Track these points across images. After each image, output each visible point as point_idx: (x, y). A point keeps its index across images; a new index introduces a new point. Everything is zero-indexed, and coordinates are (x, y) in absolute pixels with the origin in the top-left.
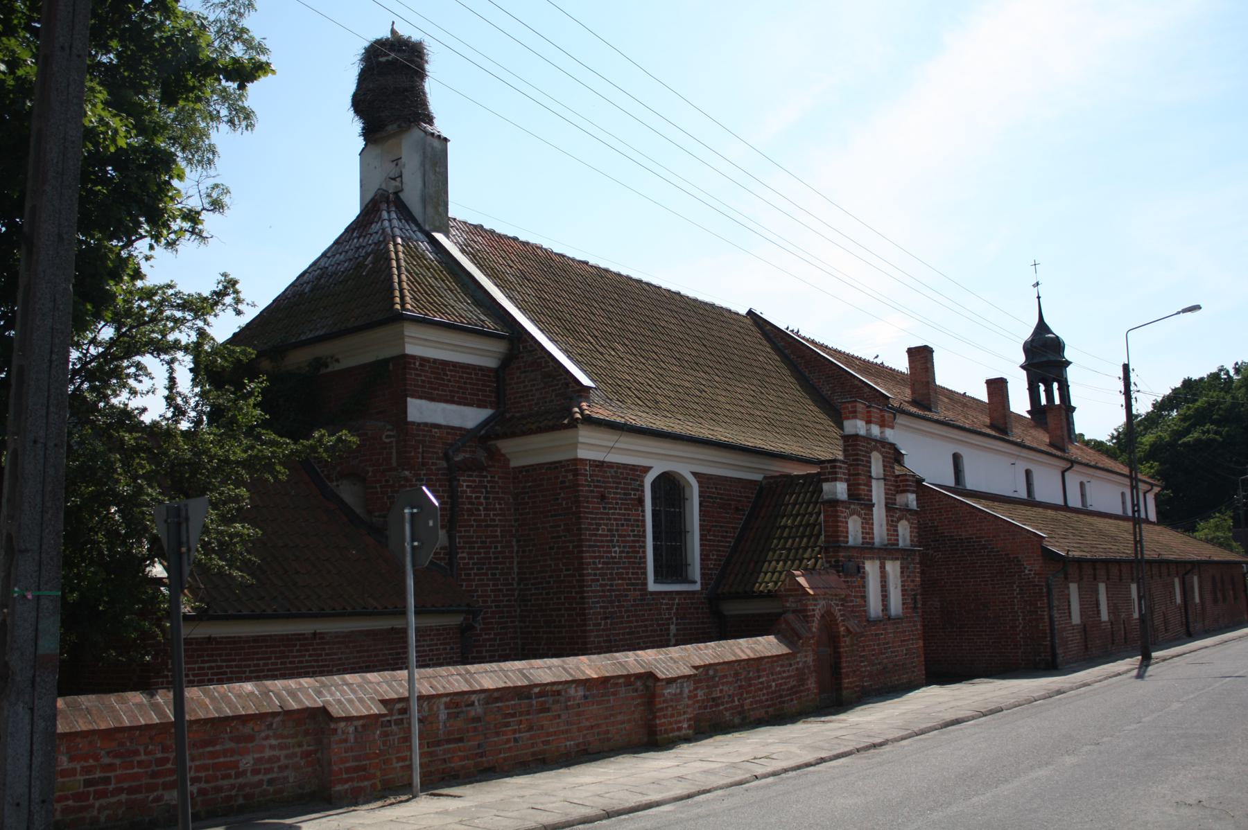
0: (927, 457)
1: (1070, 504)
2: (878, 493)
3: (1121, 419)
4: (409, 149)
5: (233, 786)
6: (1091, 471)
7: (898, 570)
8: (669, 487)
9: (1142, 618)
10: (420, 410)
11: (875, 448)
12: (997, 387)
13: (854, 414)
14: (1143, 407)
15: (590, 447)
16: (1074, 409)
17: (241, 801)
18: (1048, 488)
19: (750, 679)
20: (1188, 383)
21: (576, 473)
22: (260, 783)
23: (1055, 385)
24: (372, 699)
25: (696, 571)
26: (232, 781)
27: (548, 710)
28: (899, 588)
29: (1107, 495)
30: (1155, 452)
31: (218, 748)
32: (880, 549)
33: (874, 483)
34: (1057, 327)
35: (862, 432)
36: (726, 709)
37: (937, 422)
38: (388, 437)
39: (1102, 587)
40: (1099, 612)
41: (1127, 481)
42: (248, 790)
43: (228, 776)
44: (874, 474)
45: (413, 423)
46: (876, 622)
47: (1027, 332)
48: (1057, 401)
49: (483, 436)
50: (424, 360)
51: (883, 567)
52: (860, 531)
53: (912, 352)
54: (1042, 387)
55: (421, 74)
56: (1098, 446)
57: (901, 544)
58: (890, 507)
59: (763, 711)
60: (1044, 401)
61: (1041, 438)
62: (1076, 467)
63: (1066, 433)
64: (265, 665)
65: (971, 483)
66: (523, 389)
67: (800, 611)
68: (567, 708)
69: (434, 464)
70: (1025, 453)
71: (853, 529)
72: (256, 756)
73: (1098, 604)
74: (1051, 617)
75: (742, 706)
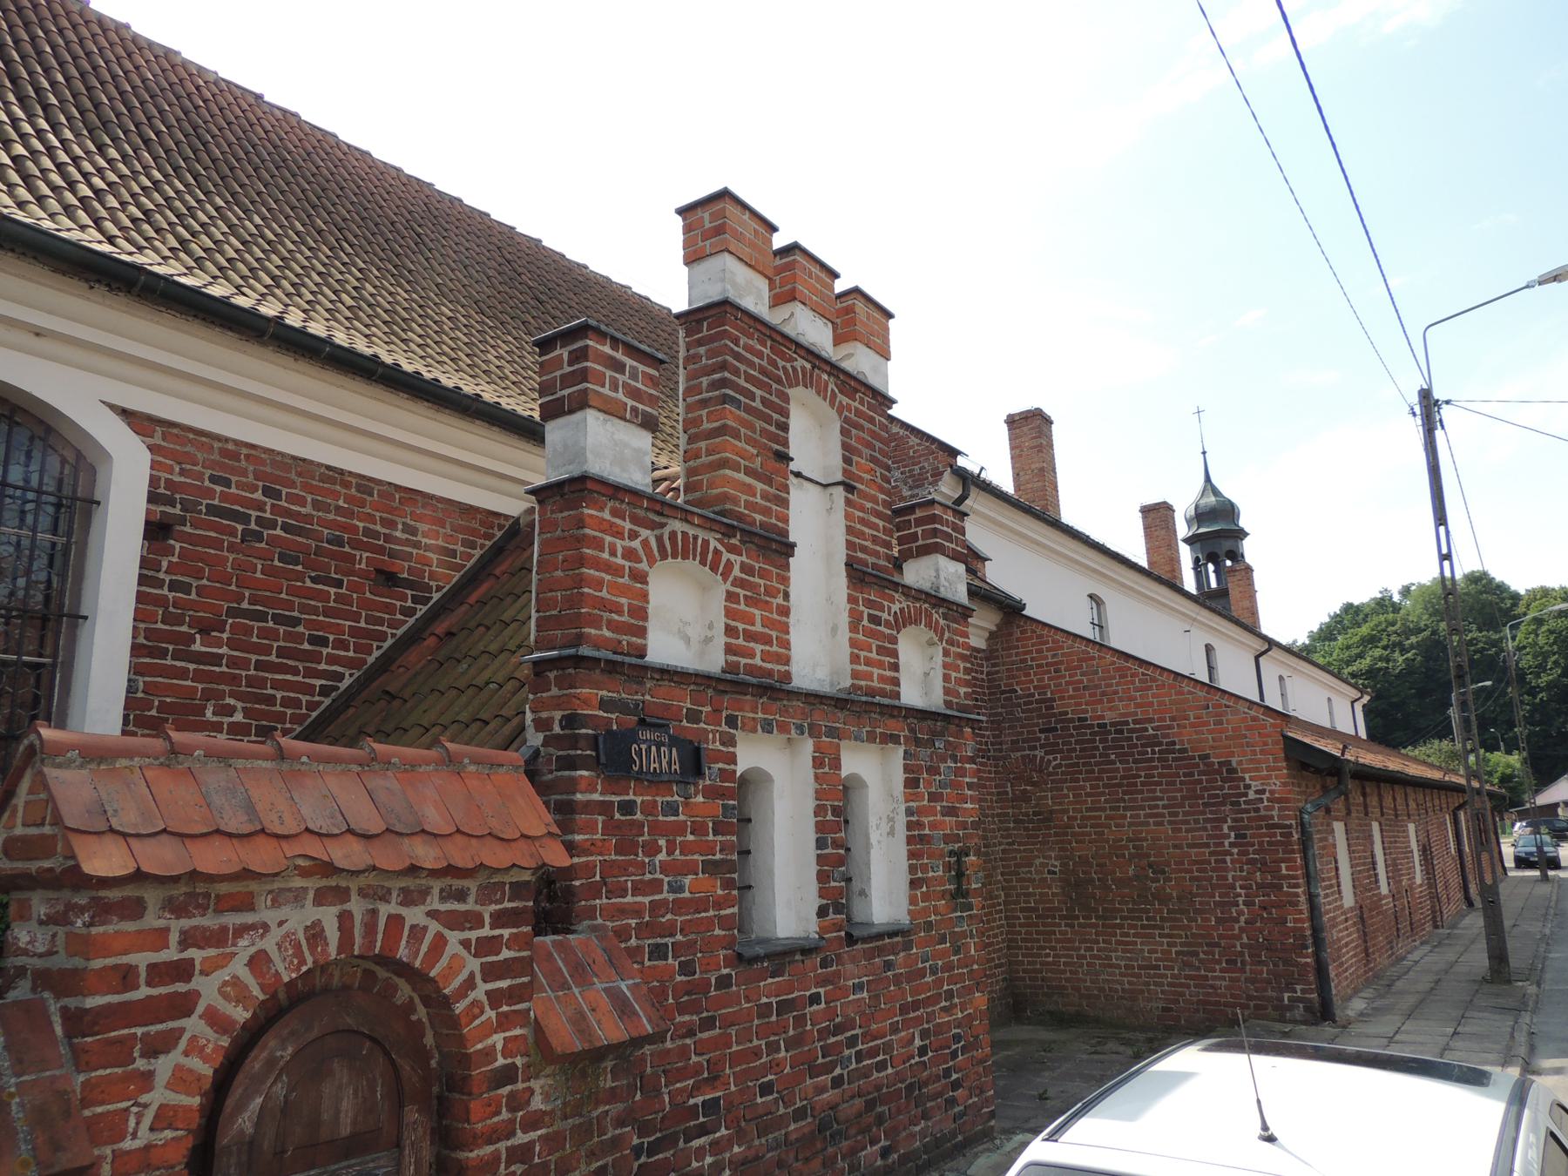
7: (899, 777)
20: (1348, 608)
28: (902, 832)
34: (1228, 492)
46: (785, 956)
51: (826, 761)
52: (720, 622)
62: (1274, 652)
74: (1311, 898)
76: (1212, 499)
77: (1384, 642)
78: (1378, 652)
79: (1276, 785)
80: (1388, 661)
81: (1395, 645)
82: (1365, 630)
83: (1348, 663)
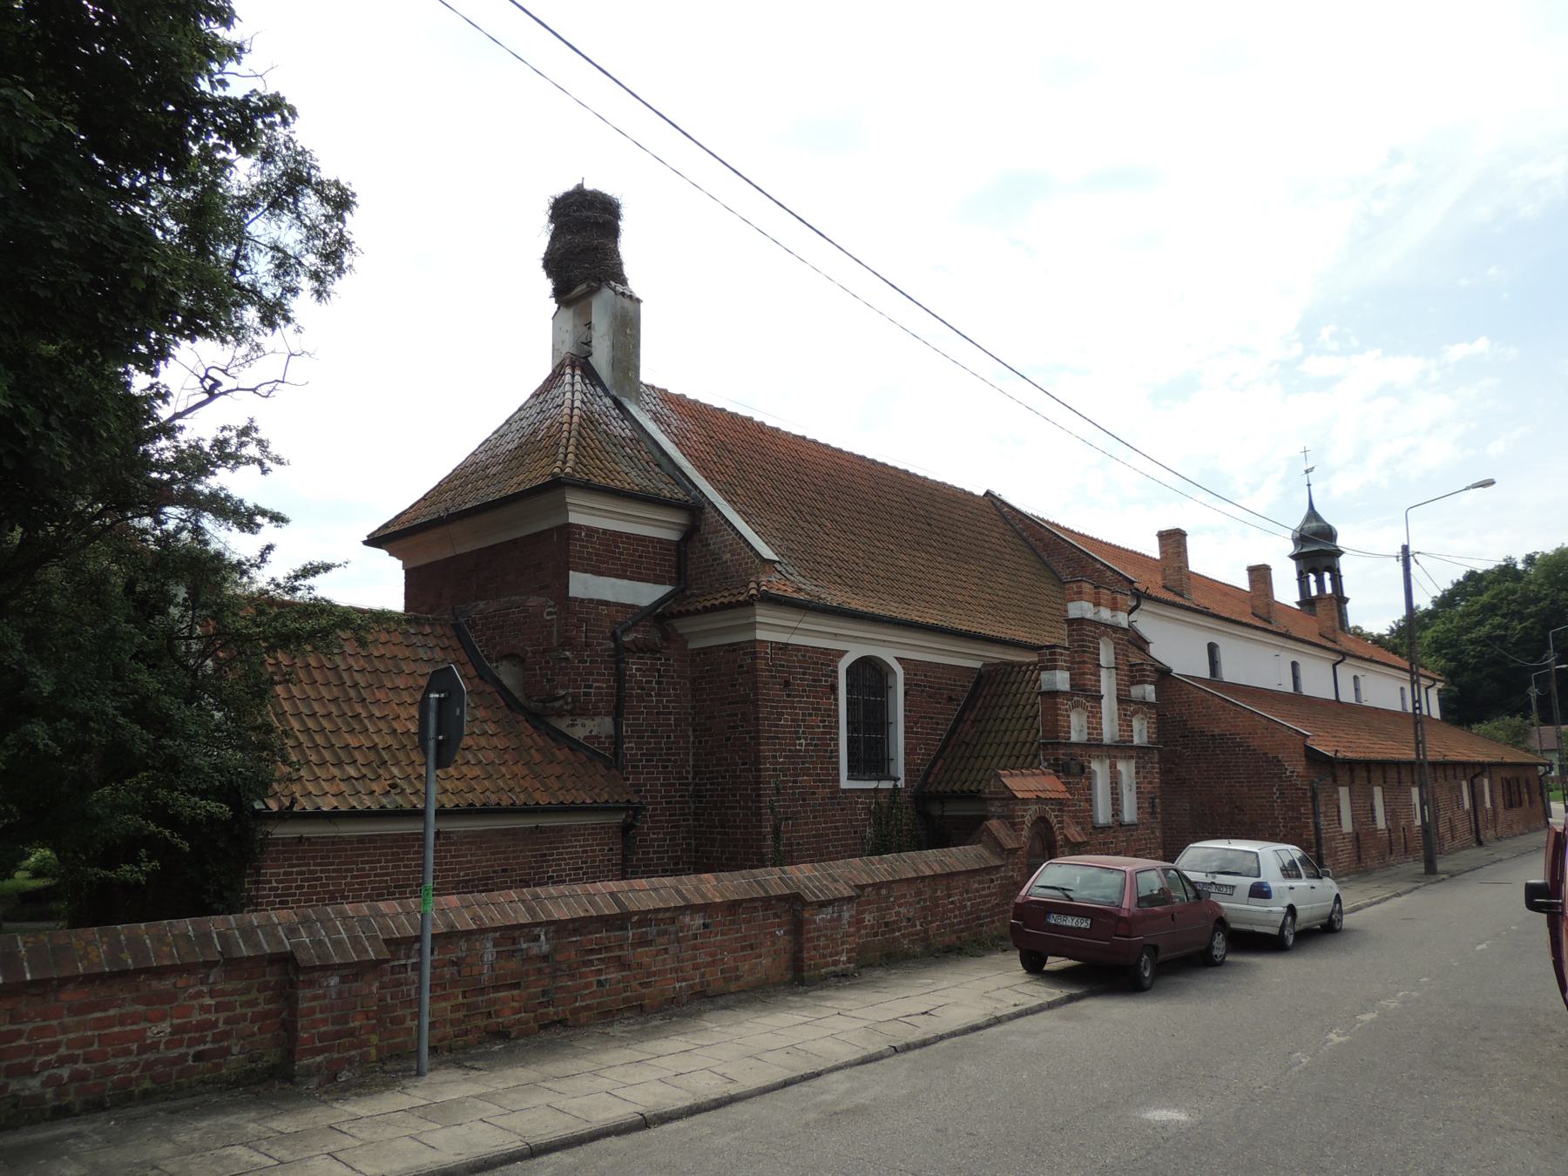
0: (1178, 647)
1: (1342, 699)
2: (1107, 684)
3: (1401, 613)
4: (601, 309)
5: (135, 1065)
6: (1366, 665)
8: (869, 675)
9: (1426, 828)
10: (583, 585)
11: (1104, 634)
12: (1260, 574)
13: (1079, 596)
14: (1423, 601)
15: (771, 628)
16: (1347, 600)
17: (147, 1084)
18: (1318, 680)
19: (938, 898)
20: (1472, 576)
21: (754, 656)
22: (183, 1057)
23: (1327, 576)
24: (373, 939)
25: (899, 767)
26: (133, 1059)
27: (650, 943)
29: (1385, 691)
30: (1438, 646)
31: (112, 1012)
32: (1109, 746)
33: (1103, 673)
34: (1328, 518)
35: (1089, 616)
36: (903, 936)
37: (1188, 609)
38: (549, 614)
39: (1378, 791)
40: (1374, 819)
41: (1407, 676)
42: (159, 1068)
43: (128, 1052)
44: (1102, 663)
45: (575, 599)
46: (1104, 828)
47: (1297, 519)
48: (1329, 590)
49: (657, 615)
50: (591, 531)
51: (1113, 766)
53: (1163, 536)
54: (1312, 578)
55: (613, 232)
56: (1378, 641)
57: (1136, 741)
58: (1123, 700)
59: (954, 937)
60: (1314, 592)
61: (1308, 627)
62: (1145, 606)
63: (1337, 624)
64: (372, 869)
65: (1229, 674)
66: (693, 560)
67: (1007, 817)
68: (679, 941)
69: (600, 644)
70: (1290, 644)
71: (1077, 729)
72: (176, 1021)
73: (1373, 810)
74: (1317, 825)
75: (926, 932)
76: (1314, 524)
77: (1505, 610)
78: (1497, 620)
79: (1300, 769)
80: (1506, 629)
81: (1514, 613)
82: (1485, 598)
83: (1467, 630)
